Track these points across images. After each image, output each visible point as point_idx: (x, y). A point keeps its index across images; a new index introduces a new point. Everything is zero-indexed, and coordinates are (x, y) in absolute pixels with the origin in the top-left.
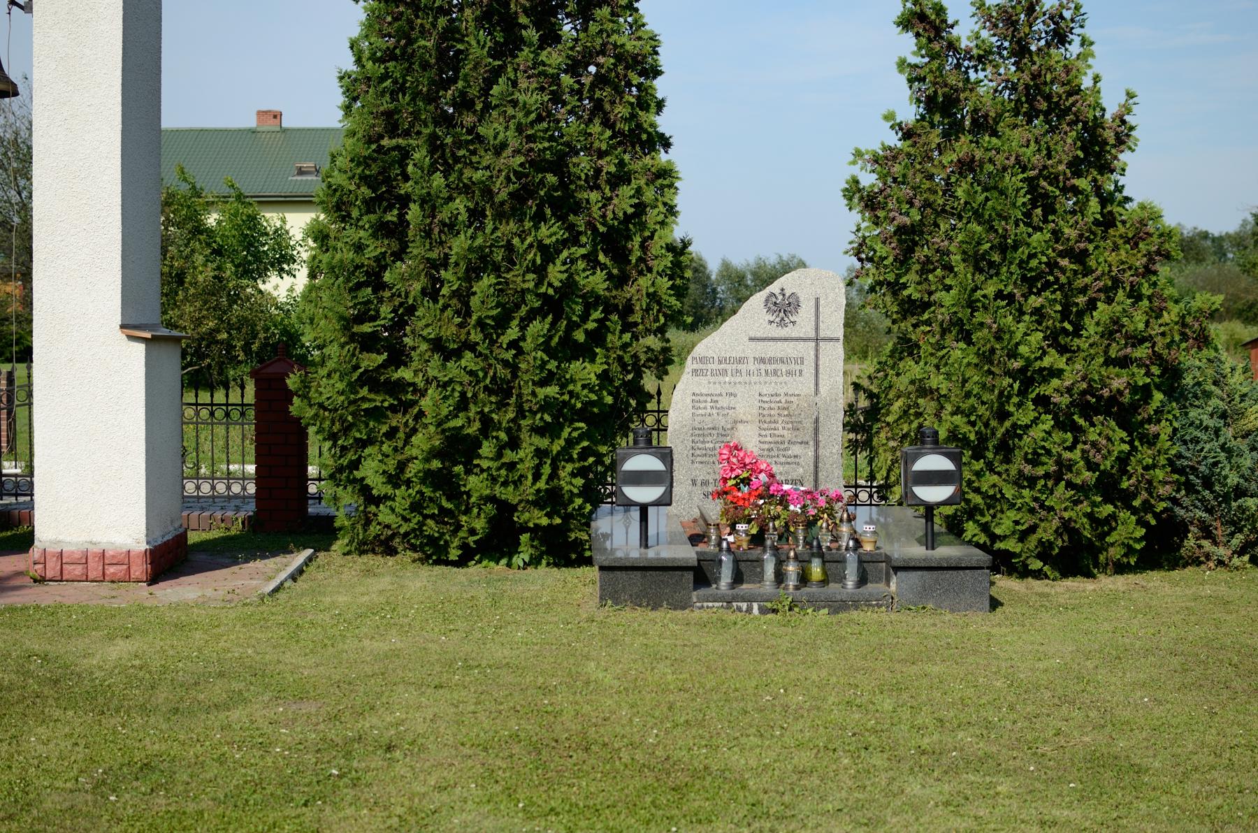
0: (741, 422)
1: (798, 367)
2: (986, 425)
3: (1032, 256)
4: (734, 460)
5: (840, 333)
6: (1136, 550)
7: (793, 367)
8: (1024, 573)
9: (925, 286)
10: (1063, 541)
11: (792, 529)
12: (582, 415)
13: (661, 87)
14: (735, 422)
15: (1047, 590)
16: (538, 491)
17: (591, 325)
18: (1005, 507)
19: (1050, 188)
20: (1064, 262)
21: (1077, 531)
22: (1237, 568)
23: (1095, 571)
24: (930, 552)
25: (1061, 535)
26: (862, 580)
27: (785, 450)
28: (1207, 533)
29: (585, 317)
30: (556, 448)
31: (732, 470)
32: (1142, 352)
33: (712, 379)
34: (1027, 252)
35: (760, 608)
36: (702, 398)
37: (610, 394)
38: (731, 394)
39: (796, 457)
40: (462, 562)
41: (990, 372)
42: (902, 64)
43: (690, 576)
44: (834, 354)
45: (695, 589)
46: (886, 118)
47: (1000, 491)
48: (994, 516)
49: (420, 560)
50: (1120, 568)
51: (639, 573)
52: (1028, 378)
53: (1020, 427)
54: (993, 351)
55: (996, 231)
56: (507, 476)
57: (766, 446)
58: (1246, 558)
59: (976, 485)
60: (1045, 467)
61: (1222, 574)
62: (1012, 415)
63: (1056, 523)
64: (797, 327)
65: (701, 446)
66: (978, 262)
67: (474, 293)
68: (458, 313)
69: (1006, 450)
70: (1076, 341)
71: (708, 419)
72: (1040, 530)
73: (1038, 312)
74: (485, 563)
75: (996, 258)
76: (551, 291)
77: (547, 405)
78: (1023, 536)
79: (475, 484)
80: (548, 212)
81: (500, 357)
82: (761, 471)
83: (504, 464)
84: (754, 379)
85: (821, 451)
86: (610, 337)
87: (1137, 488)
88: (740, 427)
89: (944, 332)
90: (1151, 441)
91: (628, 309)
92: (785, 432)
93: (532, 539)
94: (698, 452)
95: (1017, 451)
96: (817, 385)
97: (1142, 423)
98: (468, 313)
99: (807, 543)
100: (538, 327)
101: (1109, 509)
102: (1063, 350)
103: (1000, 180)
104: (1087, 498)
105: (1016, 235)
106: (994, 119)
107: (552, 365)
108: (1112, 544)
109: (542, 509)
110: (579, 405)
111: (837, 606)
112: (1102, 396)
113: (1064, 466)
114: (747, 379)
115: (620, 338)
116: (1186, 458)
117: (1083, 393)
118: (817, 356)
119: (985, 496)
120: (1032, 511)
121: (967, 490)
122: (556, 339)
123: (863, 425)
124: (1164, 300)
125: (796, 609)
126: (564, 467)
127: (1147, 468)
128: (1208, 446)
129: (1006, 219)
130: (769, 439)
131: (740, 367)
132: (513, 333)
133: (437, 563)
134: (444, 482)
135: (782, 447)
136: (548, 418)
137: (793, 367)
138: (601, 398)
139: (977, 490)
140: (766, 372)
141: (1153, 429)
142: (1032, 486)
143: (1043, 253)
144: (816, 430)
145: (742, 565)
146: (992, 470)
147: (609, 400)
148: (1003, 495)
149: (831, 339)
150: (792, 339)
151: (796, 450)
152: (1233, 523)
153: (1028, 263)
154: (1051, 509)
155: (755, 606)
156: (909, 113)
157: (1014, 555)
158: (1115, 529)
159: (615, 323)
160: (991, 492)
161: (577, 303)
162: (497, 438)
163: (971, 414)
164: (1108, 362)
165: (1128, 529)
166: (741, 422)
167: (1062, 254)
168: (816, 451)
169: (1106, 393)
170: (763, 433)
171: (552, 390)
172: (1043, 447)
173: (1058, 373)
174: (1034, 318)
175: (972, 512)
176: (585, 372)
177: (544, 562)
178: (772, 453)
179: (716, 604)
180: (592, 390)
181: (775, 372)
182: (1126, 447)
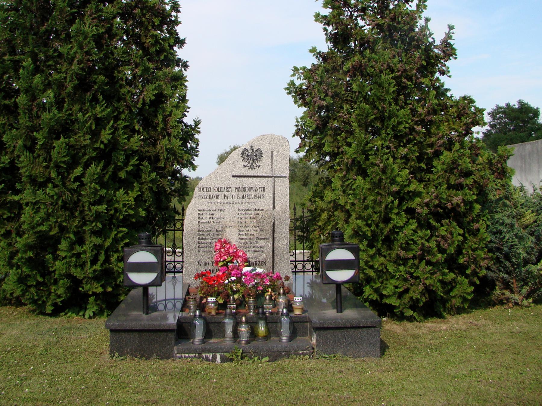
0: (228, 226)
1: (262, 193)
2: (377, 226)
3: (400, 123)
4: (222, 250)
5: (287, 173)
6: (468, 300)
7: (259, 193)
8: (401, 318)
9: (336, 144)
10: (426, 298)
11: (247, 299)
12: (125, 222)
13: (181, 31)
14: (224, 227)
15: (417, 331)
16: (95, 271)
17: (130, 168)
18: (389, 277)
19: (409, 83)
20: (418, 128)
21: (434, 292)
22: (526, 307)
23: (444, 314)
24: (339, 314)
25: (424, 295)
26: (294, 334)
27: (254, 243)
28: (507, 286)
29: (126, 164)
30: (108, 243)
31: (221, 257)
32: (469, 181)
33: (210, 201)
34: (396, 120)
35: (221, 357)
36: (204, 213)
37: (144, 210)
38: (221, 210)
39: (261, 247)
40: (56, 313)
41: (378, 193)
42: (318, 17)
43: (172, 336)
44: (284, 186)
45: (176, 344)
46: (311, 51)
47: (386, 267)
48: (382, 283)
49: (34, 311)
50: (459, 311)
51: (136, 335)
52: (403, 196)
53: (397, 227)
54: (380, 180)
55: (378, 108)
56: (76, 261)
57: (243, 241)
58: (531, 300)
59: (370, 263)
60: (414, 252)
61: (520, 312)
62: (393, 220)
63: (421, 287)
64: (261, 169)
65: (203, 241)
66: (366, 125)
67: (54, 147)
68: (45, 159)
69: (389, 241)
70: (428, 176)
71: (207, 225)
72: (411, 292)
73: (406, 159)
74: (69, 314)
75: (378, 124)
76: (102, 146)
77: (98, 216)
78: (400, 296)
79: (59, 266)
80: (101, 97)
81: (69, 187)
82: (239, 257)
83: (74, 254)
84: (236, 200)
85: (276, 244)
86: (143, 176)
87: (468, 263)
88: (227, 230)
89: (348, 170)
90: (475, 233)
91: (157, 159)
92: (255, 233)
93: (96, 300)
94: (202, 245)
95: (395, 242)
96: (273, 203)
97: (469, 223)
98: (51, 160)
99: (256, 308)
100: (94, 169)
101: (452, 275)
102: (420, 181)
103: (376, 85)
104: (440, 270)
105: (390, 111)
106: (373, 43)
107: (103, 192)
108: (454, 297)
109: (98, 282)
110: (121, 217)
111: (275, 356)
112: (447, 207)
113: (426, 251)
114: (231, 201)
115: (149, 176)
116: (495, 243)
117: (436, 206)
118: (273, 186)
119: (376, 271)
120: (406, 280)
121: (365, 267)
122: (107, 176)
123: (304, 229)
124: (478, 149)
125: (246, 358)
126: (113, 256)
127: (474, 250)
128: (507, 236)
129: (383, 101)
130: (244, 237)
131: (226, 193)
132: (78, 171)
133: (38, 314)
134: (38, 264)
135: (253, 241)
136: (100, 225)
137: (259, 193)
138: (137, 213)
139: (371, 267)
140: (243, 196)
141: (475, 226)
142: (404, 265)
143: (407, 123)
144: (273, 231)
145: (212, 326)
146: (380, 254)
147: (143, 213)
148: (387, 270)
149: (281, 176)
150: (258, 176)
151: (261, 243)
152: (523, 280)
153: (397, 127)
154: (418, 277)
155: (218, 356)
156: (325, 47)
157: (395, 307)
158: (455, 287)
159: (146, 167)
160: (380, 268)
161: (121, 155)
162: (69, 237)
163: (368, 219)
164: (450, 187)
165: (464, 288)
166: (228, 226)
167: (416, 123)
168: (273, 243)
169: (449, 205)
170: (241, 233)
171: (102, 208)
172: (412, 240)
173: (418, 194)
174: (402, 161)
175: (368, 280)
176: (125, 198)
177: (105, 314)
178: (247, 245)
179: (191, 355)
180: (130, 208)
181: (248, 197)
182: (461, 238)
